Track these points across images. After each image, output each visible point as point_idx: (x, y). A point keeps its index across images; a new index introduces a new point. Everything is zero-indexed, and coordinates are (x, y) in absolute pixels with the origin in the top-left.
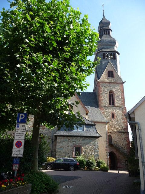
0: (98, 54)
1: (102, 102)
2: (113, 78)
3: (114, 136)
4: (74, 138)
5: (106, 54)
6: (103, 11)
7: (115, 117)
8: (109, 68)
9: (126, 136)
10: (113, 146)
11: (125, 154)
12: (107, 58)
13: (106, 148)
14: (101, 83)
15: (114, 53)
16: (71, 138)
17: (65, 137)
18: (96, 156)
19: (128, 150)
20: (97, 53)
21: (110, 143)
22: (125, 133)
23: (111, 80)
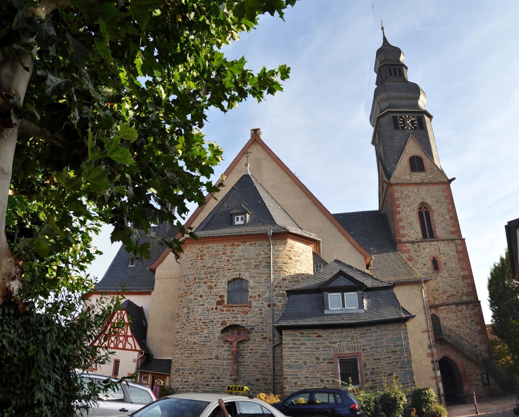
0: (381, 120)
1: (405, 232)
2: (423, 174)
3: (445, 315)
4: (336, 331)
5: (401, 117)
6: (382, 29)
7: (441, 266)
8: (412, 148)
9: (475, 311)
10: (446, 342)
11: (477, 356)
12: (403, 128)
13: (429, 351)
14: (395, 188)
15: (420, 115)
16: (324, 333)
17: (305, 332)
18: (408, 376)
19: (484, 345)
20: (379, 118)
21: (438, 334)
22: (471, 305)
23: (418, 177)
